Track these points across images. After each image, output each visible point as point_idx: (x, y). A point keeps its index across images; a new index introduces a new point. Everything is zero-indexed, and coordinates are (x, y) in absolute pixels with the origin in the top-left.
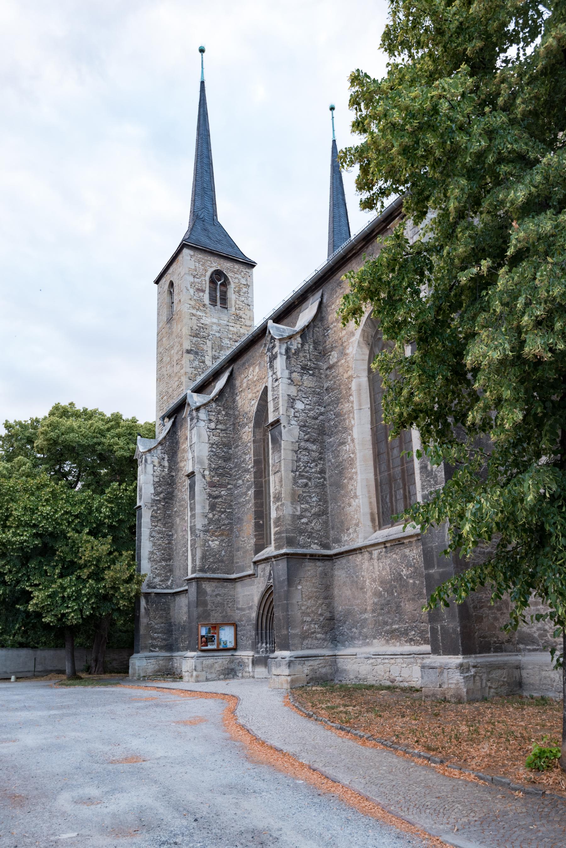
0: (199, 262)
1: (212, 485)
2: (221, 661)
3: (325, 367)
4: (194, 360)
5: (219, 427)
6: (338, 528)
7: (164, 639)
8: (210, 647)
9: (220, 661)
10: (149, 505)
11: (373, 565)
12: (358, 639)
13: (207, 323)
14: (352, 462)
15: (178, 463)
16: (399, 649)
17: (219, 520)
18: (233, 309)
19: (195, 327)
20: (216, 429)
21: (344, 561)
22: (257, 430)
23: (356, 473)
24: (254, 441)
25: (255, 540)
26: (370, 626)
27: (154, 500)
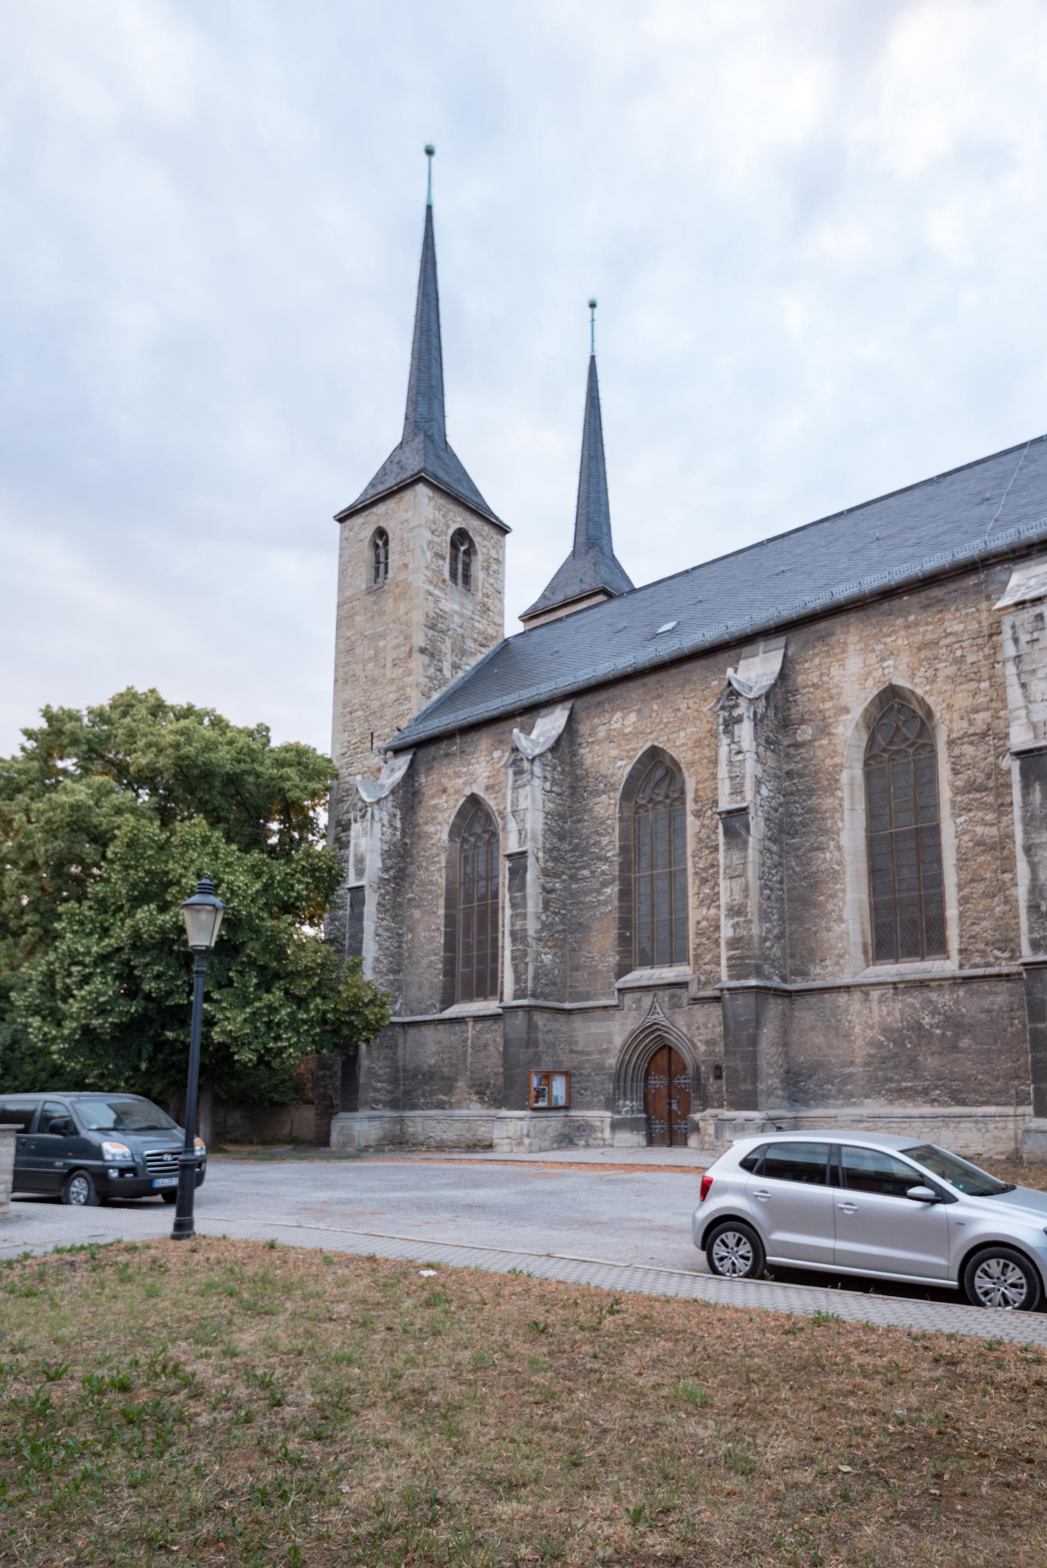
0: (440, 510)
1: (546, 873)
2: (554, 1123)
3: (786, 743)
4: (429, 665)
5: (555, 789)
6: (802, 957)
7: (390, 1092)
8: (541, 1104)
9: (553, 1123)
10: (375, 886)
11: (870, 1008)
12: (835, 1098)
13: (447, 609)
14: (836, 876)
15: (418, 825)
16: (911, 1110)
17: (552, 924)
18: (480, 594)
19: (432, 614)
20: (551, 791)
21: (813, 1000)
22: (625, 804)
23: (844, 891)
24: (621, 819)
25: (617, 958)
26: (860, 1083)
27: (382, 879)
